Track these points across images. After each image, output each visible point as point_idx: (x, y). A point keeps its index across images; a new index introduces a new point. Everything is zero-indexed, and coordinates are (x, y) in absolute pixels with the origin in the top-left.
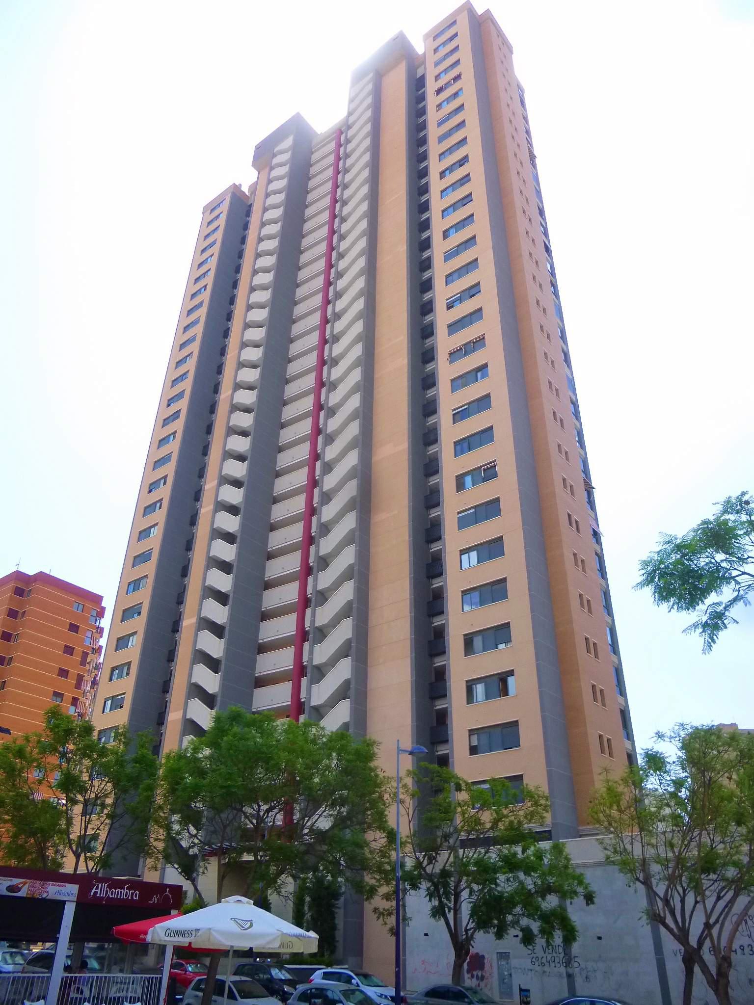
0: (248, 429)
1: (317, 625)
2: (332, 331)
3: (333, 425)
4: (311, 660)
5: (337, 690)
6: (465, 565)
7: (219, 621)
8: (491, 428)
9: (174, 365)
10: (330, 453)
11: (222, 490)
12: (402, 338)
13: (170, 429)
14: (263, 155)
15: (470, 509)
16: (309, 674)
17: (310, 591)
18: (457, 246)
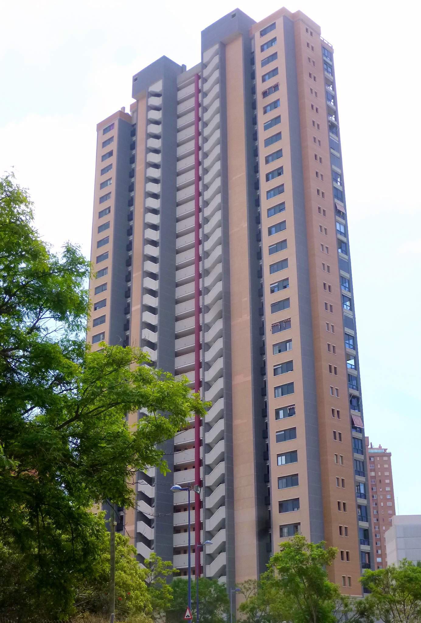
0: (159, 164)
1: (205, 286)
2: (203, 266)
3: (206, 87)
4: (204, 359)
5: (218, 547)
6: (280, 463)
7: (155, 239)
8: (285, 221)
9: (100, 159)
10: (206, 117)
11: (147, 160)
12: (246, 299)
13: (108, 136)
14: (141, 82)
15: (279, 365)
16: (203, 386)
17: (201, 269)
18: (272, 120)
